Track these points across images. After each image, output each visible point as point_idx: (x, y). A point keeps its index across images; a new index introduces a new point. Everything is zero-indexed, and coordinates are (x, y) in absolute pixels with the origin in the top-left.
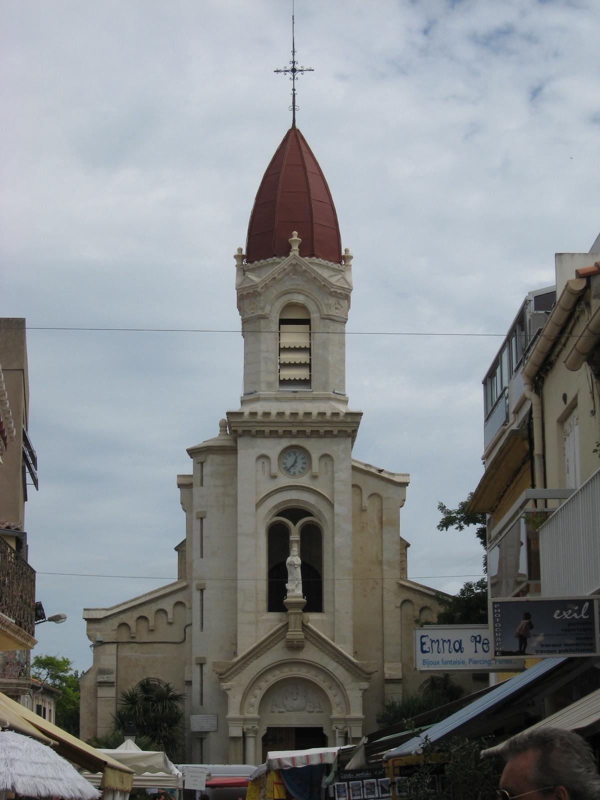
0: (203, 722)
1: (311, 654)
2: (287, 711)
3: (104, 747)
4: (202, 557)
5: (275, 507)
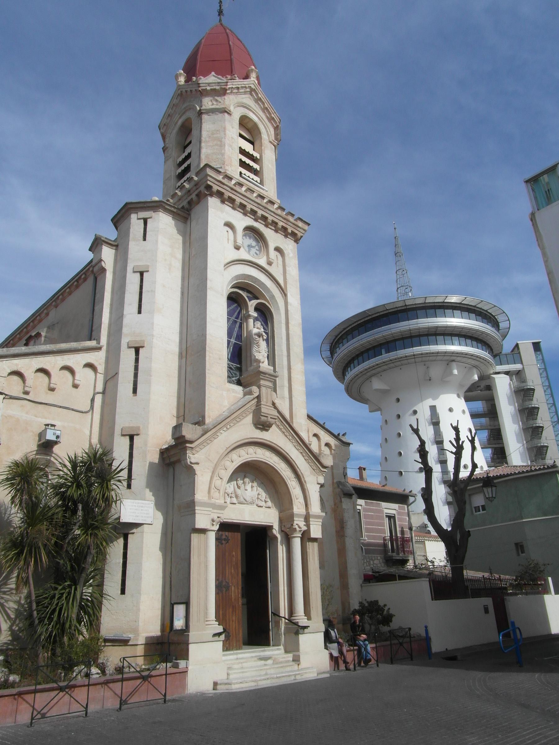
0: (137, 509)
1: (274, 436)
2: (238, 503)
3: (218, 582)
4: (140, 312)
5: (237, 277)
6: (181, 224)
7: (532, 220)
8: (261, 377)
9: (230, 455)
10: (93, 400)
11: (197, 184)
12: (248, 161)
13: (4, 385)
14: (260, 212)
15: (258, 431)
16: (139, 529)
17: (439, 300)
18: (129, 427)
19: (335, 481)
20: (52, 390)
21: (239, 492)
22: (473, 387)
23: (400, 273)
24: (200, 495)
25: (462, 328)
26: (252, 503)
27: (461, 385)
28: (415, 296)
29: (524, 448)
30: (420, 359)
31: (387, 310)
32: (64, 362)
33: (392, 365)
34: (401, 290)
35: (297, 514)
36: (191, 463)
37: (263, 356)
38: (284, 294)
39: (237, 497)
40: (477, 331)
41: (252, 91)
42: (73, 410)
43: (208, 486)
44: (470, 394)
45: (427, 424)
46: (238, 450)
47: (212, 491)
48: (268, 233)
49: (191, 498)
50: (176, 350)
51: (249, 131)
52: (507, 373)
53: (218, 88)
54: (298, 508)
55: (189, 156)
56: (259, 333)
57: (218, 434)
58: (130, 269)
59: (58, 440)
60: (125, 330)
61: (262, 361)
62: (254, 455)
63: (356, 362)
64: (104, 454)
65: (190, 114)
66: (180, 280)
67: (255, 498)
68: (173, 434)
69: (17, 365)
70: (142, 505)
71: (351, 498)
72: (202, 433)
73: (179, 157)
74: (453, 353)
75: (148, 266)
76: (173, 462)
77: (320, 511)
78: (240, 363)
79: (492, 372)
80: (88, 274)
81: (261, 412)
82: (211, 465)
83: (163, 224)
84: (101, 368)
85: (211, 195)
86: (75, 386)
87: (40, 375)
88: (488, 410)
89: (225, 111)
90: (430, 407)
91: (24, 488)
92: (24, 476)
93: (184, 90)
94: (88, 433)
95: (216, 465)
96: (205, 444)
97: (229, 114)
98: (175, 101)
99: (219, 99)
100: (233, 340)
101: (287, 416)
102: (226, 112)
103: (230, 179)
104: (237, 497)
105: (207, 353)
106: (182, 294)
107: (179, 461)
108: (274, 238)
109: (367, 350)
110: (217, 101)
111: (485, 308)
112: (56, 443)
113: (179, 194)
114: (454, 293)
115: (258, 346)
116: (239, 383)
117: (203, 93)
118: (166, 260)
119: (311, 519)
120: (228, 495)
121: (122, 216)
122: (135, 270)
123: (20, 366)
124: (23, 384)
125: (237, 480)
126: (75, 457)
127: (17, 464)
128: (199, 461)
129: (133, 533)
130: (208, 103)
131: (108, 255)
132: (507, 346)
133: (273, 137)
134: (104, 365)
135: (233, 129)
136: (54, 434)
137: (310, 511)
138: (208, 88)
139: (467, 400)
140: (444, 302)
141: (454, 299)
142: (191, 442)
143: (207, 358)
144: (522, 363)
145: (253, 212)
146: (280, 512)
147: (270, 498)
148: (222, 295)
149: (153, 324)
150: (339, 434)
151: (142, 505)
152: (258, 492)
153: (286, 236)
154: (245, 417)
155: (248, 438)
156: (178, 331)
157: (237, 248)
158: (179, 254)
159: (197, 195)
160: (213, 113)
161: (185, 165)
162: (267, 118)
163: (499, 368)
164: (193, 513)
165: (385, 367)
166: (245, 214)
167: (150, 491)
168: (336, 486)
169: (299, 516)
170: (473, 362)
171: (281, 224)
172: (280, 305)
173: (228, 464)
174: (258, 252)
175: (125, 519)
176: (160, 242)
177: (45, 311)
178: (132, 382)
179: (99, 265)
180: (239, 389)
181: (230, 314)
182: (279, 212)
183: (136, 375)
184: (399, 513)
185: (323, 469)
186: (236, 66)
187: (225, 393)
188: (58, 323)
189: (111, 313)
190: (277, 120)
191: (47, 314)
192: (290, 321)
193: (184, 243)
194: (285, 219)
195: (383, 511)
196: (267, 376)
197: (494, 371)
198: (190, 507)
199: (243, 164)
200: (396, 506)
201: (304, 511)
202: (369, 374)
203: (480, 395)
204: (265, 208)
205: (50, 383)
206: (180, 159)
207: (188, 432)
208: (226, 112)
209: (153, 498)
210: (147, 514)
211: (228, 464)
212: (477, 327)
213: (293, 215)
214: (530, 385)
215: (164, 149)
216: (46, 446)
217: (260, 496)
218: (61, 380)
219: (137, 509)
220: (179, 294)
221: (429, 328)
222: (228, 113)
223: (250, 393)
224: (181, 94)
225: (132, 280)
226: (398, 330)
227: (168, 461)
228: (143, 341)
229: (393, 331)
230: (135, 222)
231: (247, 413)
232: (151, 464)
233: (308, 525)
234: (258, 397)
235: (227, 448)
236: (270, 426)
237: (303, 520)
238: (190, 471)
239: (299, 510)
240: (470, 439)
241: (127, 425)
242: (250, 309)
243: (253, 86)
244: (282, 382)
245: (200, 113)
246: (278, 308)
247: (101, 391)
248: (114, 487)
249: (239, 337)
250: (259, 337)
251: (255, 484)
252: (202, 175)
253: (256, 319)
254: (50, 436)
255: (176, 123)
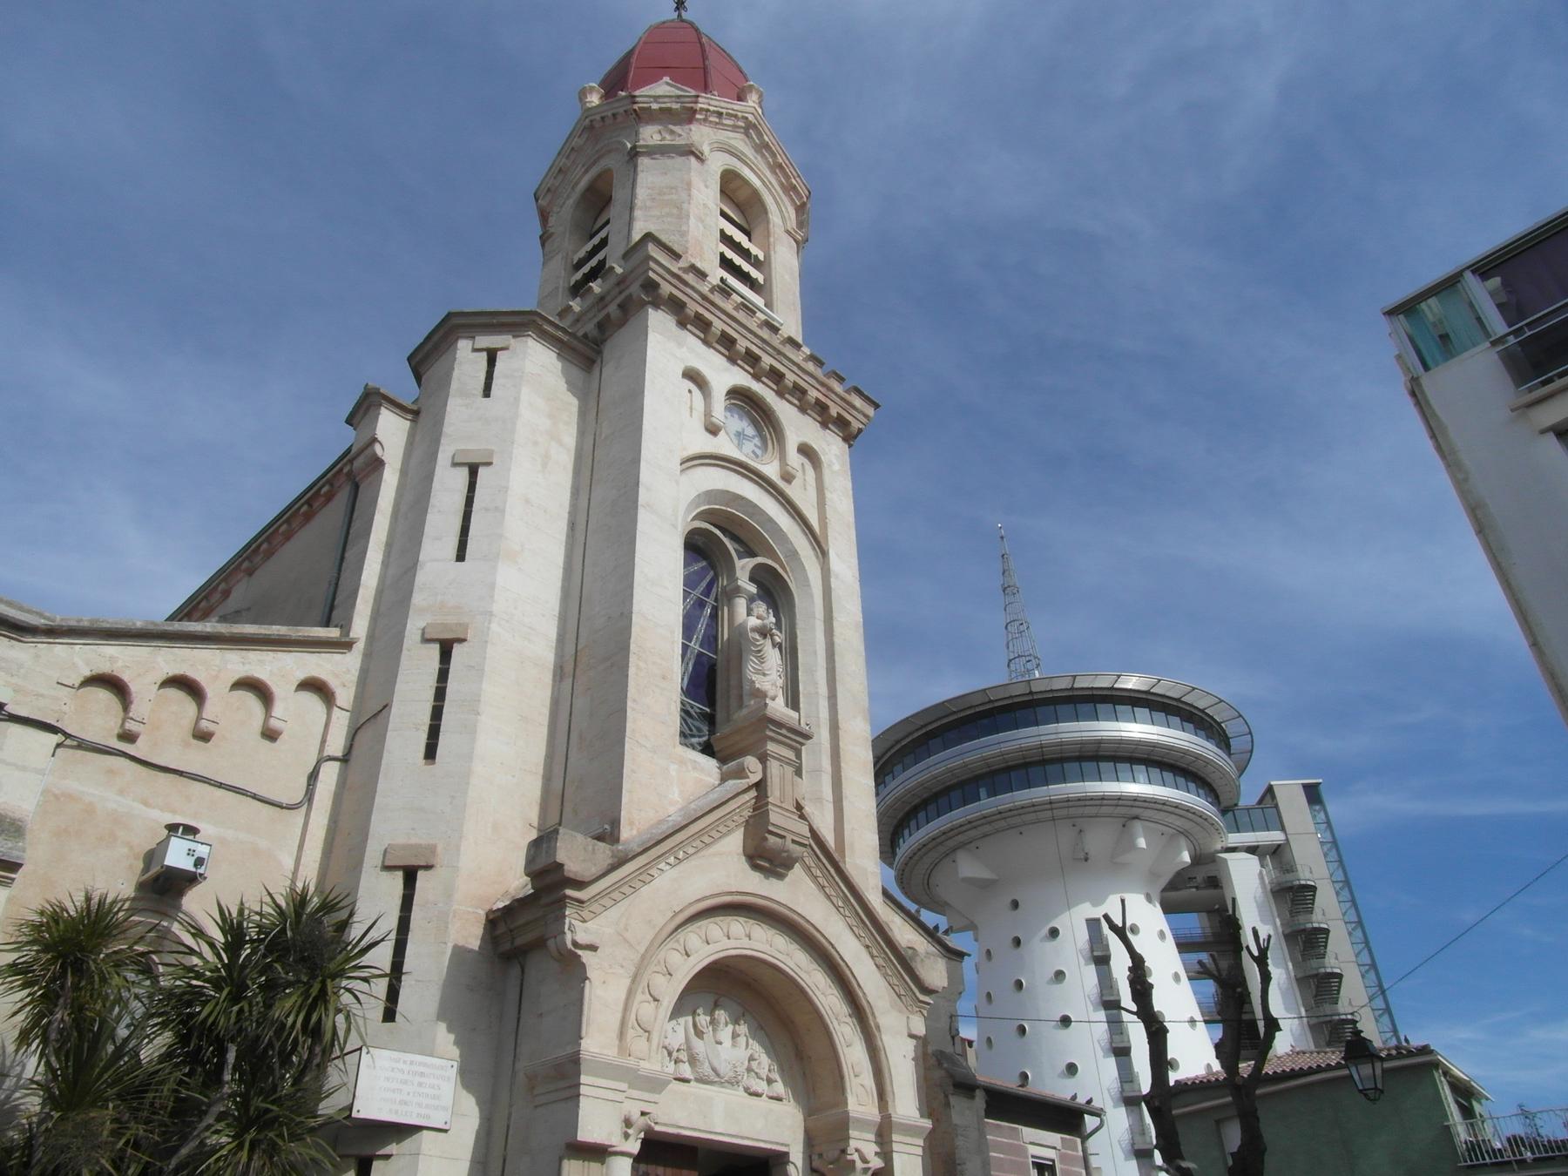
0: (405, 1082)
1: (799, 893)
2: (697, 1080)
4: (461, 557)
5: (710, 495)
6: (576, 373)
7: (1413, 394)
8: (769, 733)
9: (681, 935)
10: (313, 777)
11: (622, 281)
12: (738, 261)
13: (65, 708)
14: (767, 361)
15: (756, 877)
16: (409, 1144)
17: (1103, 682)
18: (406, 847)
19: (930, 1049)
20: (204, 736)
21: (699, 1046)
22: (1179, 881)
23: (1013, 628)
24: (597, 1041)
25: (1154, 745)
26: (733, 1082)
27: (1153, 875)
28: (1048, 675)
29: (1301, 1024)
30: (1064, 812)
31: (991, 701)
32: (247, 667)
33: (1003, 824)
34: (1019, 665)
35: (858, 1120)
36: (575, 944)
37: (774, 684)
38: (819, 546)
39: (693, 1061)
40: (1186, 752)
41: (749, 128)
42: (255, 797)
43: (619, 1016)
44: (1173, 895)
45: (1082, 962)
46: (703, 923)
47: (630, 1033)
48: (785, 411)
49: (570, 1050)
50: (549, 657)
51: (740, 201)
52: (1252, 850)
53: (675, 106)
54: (860, 1101)
55: (604, 243)
56: (764, 626)
57: (654, 872)
58: (444, 458)
59: (201, 871)
60: (418, 599)
61: (771, 693)
62: (745, 942)
63: (922, 815)
64: (327, 907)
65: (609, 162)
66: (568, 494)
67: (742, 1069)
68: (530, 861)
69: (112, 659)
70: (422, 1069)
71: (973, 1097)
72: (610, 861)
73: (575, 252)
74: (1136, 800)
75: (491, 453)
76: (525, 948)
77: (917, 1114)
78: (711, 702)
79: (1219, 846)
80: (337, 484)
81: (768, 822)
82: (630, 956)
83: (534, 365)
84: (345, 696)
85: (656, 306)
86: (270, 735)
87: (175, 694)
88: (1214, 934)
89: (690, 152)
90: (1088, 921)
91: (62, 987)
92: (70, 952)
93: (598, 117)
94: (289, 863)
95: (643, 957)
96: (616, 895)
97: (700, 158)
98: (577, 142)
99: (677, 129)
100: (695, 646)
101: (829, 838)
102: (692, 153)
103: (702, 275)
104: (693, 1061)
105: (633, 658)
106: (572, 526)
107: (540, 944)
108: (797, 426)
109: (947, 790)
110: (672, 132)
111: (1201, 704)
112: (191, 879)
113: (577, 308)
114: (1134, 669)
115: (762, 659)
116: (707, 749)
117: (644, 116)
118: (536, 443)
119: (895, 1137)
120: (670, 1054)
121: (436, 348)
122: (457, 460)
123: (120, 664)
124: (121, 714)
125: (694, 1013)
126: (241, 912)
127: (55, 917)
128: (596, 941)
129: (388, 1157)
130: (650, 134)
131: (391, 430)
132: (1249, 795)
133: (792, 222)
134: (353, 690)
135: (705, 197)
136: (190, 852)
137: (891, 1111)
138: (655, 106)
139: (1168, 908)
140: (1112, 688)
141: (1131, 682)
142: (581, 885)
143: (632, 671)
144: (1283, 829)
145: (751, 359)
146: (809, 1113)
147: (782, 1071)
148: (675, 526)
149: (492, 586)
150: (936, 928)
151: (422, 1069)
152: (750, 1052)
153: (824, 425)
154: (725, 835)
155: (731, 893)
156: (556, 613)
157: (713, 430)
158: (570, 437)
159: (622, 307)
160: (662, 154)
161: (593, 262)
162: (782, 185)
163: (1234, 839)
164: (572, 1095)
165: (987, 828)
166: (732, 360)
167: (450, 1030)
168: (933, 1061)
169: (863, 1124)
170: (1179, 822)
171: (813, 394)
172: (811, 576)
173: (675, 958)
174: (759, 452)
175: (370, 1107)
176: (524, 406)
177: (223, 586)
178: (426, 728)
179: (367, 452)
180: (710, 764)
181: (690, 583)
182: (810, 366)
183: (437, 713)
184: (1063, 1158)
185: (922, 997)
186: (714, 76)
187: (673, 769)
188: (249, 609)
189: (385, 564)
190: (803, 192)
191: (226, 594)
192: (835, 614)
193: (582, 414)
194: (823, 384)
195: (1026, 1150)
196: (784, 731)
197: (1224, 845)
198: (564, 1077)
199: (726, 263)
200: (1054, 1138)
201: (876, 1111)
202: (951, 843)
203: (1197, 897)
204: (779, 353)
205: (199, 718)
206: (582, 254)
207: (575, 854)
208: (692, 153)
209: (456, 1052)
210: (434, 1097)
211: (675, 958)
212: (1184, 745)
213: (841, 379)
214: (1304, 876)
215: (544, 239)
216: (165, 887)
217: (754, 1065)
218: (233, 714)
219: (405, 1082)
220: (563, 525)
221: (1083, 743)
222: (698, 157)
223: (740, 773)
224: (591, 127)
225: (448, 485)
226: (1014, 745)
227: (507, 946)
228: (465, 627)
229: (1005, 747)
230: (467, 359)
231: (729, 823)
232: (459, 952)
233: (886, 1154)
234: (760, 786)
235: (676, 914)
236: (788, 863)
237: (872, 1137)
238: (571, 968)
239: (861, 1109)
240: (1256, 953)
241: (401, 840)
242: (739, 573)
243: (751, 117)
244: (816, 754)
245: (634, 154)
246: (806, 582)
247: (339, 754)
248: (346, 998)
249: (711, 639)
250: (764, 636)
251: (743, 1029)
252: (636, 258)
253: (751, 600)
254: (178, 856)
255: (577, 184)
